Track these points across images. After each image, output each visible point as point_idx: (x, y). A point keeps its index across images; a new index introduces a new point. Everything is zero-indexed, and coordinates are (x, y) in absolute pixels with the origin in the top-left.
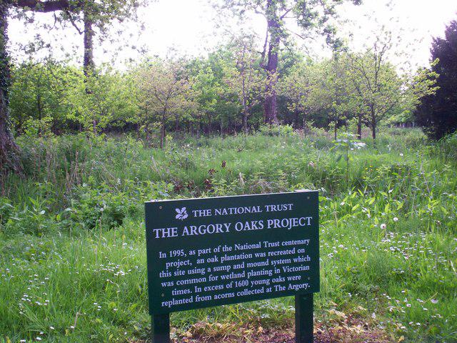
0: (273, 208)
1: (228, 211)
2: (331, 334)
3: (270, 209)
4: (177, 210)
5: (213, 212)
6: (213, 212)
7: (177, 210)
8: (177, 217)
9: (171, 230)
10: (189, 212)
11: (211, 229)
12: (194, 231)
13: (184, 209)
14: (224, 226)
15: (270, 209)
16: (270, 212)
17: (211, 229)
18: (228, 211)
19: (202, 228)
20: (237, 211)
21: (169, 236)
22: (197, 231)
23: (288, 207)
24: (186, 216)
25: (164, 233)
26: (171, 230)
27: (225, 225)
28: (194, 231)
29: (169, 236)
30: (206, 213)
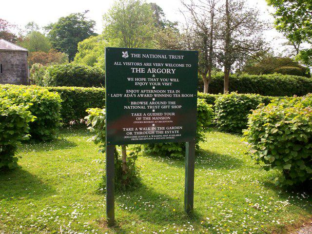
0: (173, 57)
1: (150, 56)
2: (100, 139)
3: (171, 57)
4: (123, 53)
5: (141, 56)
6: (141, 56)
7: (123, 53)
8: (123, 56)
9: (141, 71)
10: (129, 54)
11: (164, 71)
12: (138, 64)
13: (126, 52)
14: (171, 70)
15: (171, 57)
16: (171, 59)
17: (164, 71)
18: (150, 56)
19: (159, 70)
20: (154, 56)
21: (140, 72)
22: (156, 71)
23: (181, 57)
24: (127, 56)
25: (137, 70)
26: (141, 71)
27: (172, 70)
28: (138, 64)
29: (140, 72)
30: (138, 56)
